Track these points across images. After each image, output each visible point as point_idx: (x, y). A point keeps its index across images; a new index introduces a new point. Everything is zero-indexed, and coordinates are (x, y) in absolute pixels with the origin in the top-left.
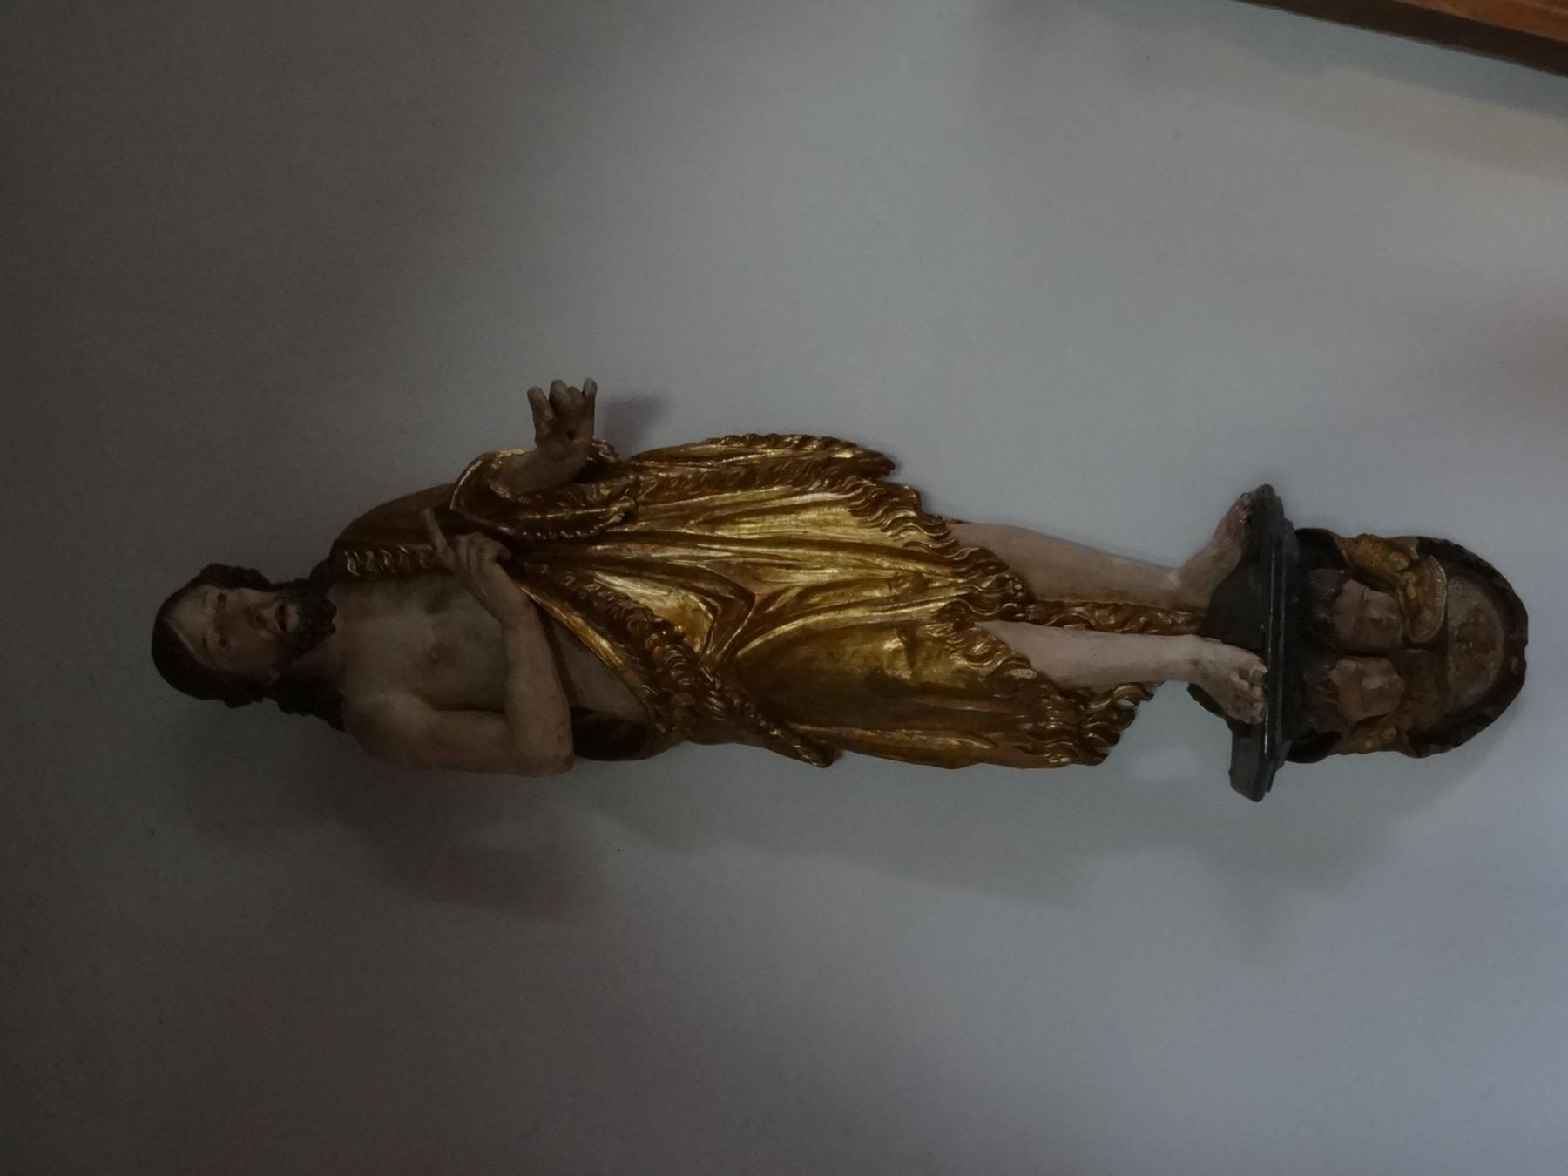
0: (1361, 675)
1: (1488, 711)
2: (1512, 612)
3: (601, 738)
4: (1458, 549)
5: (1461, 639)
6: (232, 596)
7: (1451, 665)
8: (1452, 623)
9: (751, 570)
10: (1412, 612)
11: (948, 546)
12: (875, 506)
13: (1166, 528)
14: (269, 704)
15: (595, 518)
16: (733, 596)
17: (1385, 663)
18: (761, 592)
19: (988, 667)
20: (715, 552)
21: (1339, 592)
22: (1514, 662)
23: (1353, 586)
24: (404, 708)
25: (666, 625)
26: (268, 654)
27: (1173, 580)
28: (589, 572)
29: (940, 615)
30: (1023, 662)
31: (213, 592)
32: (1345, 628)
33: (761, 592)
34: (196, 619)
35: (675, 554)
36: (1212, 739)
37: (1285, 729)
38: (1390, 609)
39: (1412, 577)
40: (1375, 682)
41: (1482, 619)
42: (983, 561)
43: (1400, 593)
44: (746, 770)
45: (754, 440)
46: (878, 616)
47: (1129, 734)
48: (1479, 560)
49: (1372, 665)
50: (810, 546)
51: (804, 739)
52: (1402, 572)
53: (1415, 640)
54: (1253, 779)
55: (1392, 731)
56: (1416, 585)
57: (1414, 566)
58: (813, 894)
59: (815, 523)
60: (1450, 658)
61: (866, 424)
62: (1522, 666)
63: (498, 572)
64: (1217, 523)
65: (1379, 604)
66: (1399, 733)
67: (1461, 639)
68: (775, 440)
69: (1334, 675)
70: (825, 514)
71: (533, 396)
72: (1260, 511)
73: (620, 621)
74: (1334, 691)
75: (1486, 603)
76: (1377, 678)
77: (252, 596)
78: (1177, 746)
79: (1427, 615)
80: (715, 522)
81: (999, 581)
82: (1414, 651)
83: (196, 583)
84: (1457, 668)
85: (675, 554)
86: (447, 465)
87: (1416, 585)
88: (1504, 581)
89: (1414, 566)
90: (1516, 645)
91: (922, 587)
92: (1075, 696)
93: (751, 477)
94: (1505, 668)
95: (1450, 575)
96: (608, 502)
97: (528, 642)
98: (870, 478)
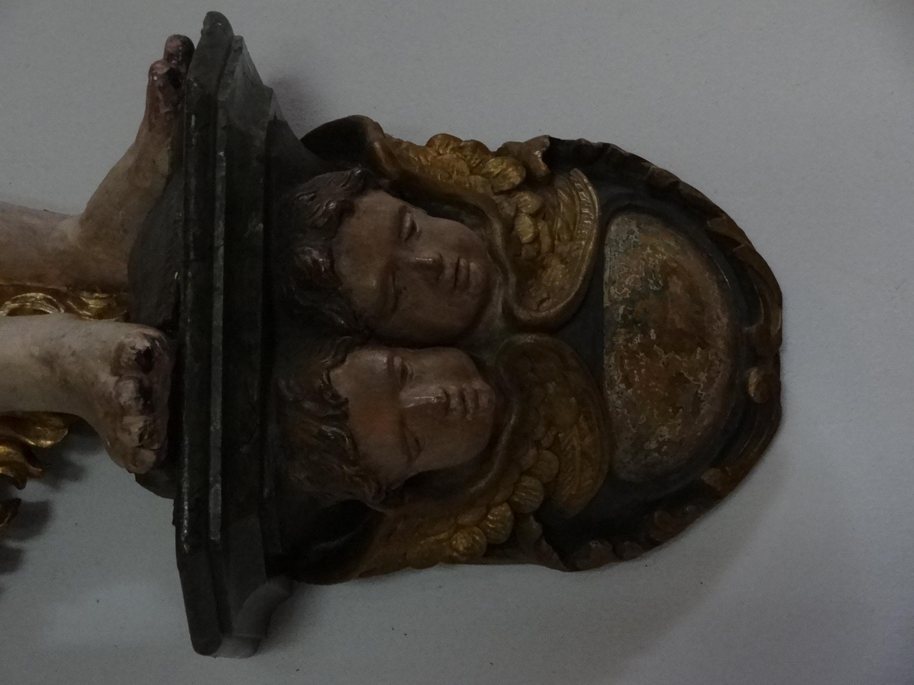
0: (400, 378)
1: (709, 476)
2: (753, 289)
4: (634, 163)
5: (631, 323)
7: (616, 375)
8: (612, 293)
17: (453, 357)
21: (346, 210)
23: (380, 205)
27: (70, 230)
28: (12, 544)
32: (365, 281)
38: (464, 249)
39: (529, 201)
40: (424, 392)
41: (676, 287)
43: (497, 227)
48: (676, 182)
49: (429, 361)
52: (509, 193)
53: (523, 314)
55: (504, 510)
56: (534, 216)
57: (530, 182)
60: (610, 360)
65: (436, 238)
66: (519, 517)
67: (631, 323)
69: (343, 380)
74: (338, 410)
75: (691, 262)
76: (432, 382)
79: (556, 273)
82: (528, 339)
84: (627, 380)
87: (534, 216)
88: (731, 223)
89: (530, 182)
90: (760, 346)
94: (735, 385)
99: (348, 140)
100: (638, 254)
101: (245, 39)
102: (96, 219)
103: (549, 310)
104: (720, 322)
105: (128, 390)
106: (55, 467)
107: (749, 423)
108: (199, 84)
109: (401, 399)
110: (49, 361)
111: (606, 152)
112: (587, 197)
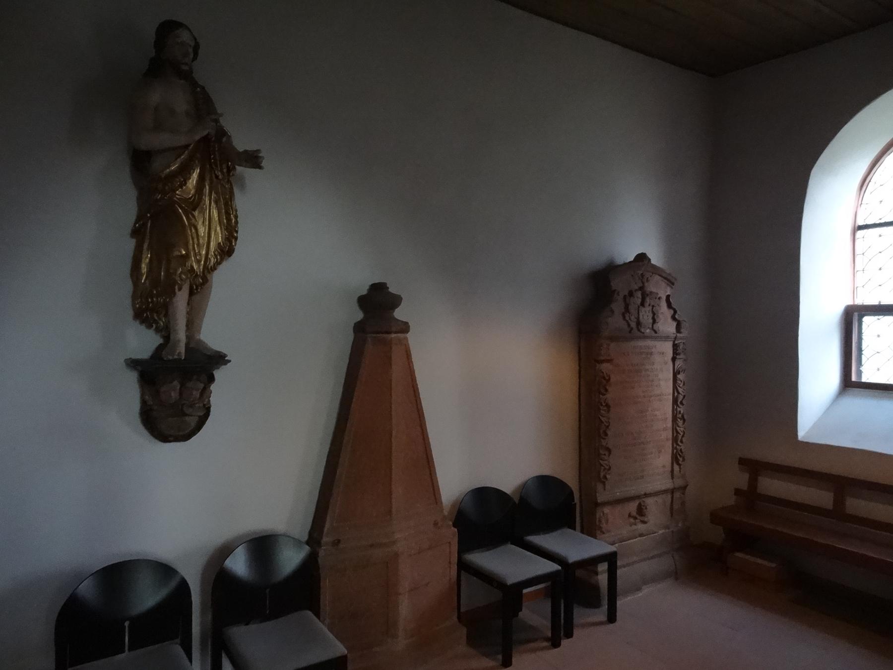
3: (140, 161)
6: (191, 50)
9: (202, 212)
10: (191, 406)
11: (209, 270)
12: (222, 251)
13: (213, 334)
14: (153, 54)
15: (216, 166)
16: (195, 204)
18: (196, 213)
19: (178, 279)
20: (207, 202)
22: (171, 439)
23: (202, 386)
24: (155, 97)
25: (186, 183)
26: (168, 56)
29: (192, 267)
30: (180, 289)
31: (193, 44)
32: (190, 385)
33: (196, 213)
34: (185, 36)
35: (207, 189)
36: (145, 353)
37: (151, 372)
39: (201, 405)
42: (205, 280)
44: (126, 208)
45: (236, 217)
46: (191, 247)
47: (143, 327)
50: (206, 229)
51: (144, 225)
54: (133, 364)
57: (204, 405)
58: (86, 226)
59: (216, 231)
61: (239, 247)
62: (170, 441)
63: (205, 133)
64: (218, 350)
65: (196, 394)
68: (237, 222)
70: (218, 236)
71: (258, 151)
72: (220, 359)
73: (184, 171)
76: (174, 395)
77: (192, 56)
78: (142, 342)
80: (216, 202)
81: (199, 285)
83: (195, 39)
85: (207, 189)
86: (227, 124)
89: (204, 405)
91: (198, 262)
92: (166, 309)
93: (228, 214)
94: (171, 436)
95: (200, 417)
96: (221, 171)
97: (182, 140)
98: (226, 251)
99: (211, 379)
100: (192, 421)
101: (129, 231)
102: (200, 342)
103: (185, 409)
104: (181, 433)
105: (176, 357)
106: (158, 330)
107: (164, 437)
108: (220, 359)
109: (172, 391)
110: (179, 341)
111: (209, 415)
112: (201, 414)
